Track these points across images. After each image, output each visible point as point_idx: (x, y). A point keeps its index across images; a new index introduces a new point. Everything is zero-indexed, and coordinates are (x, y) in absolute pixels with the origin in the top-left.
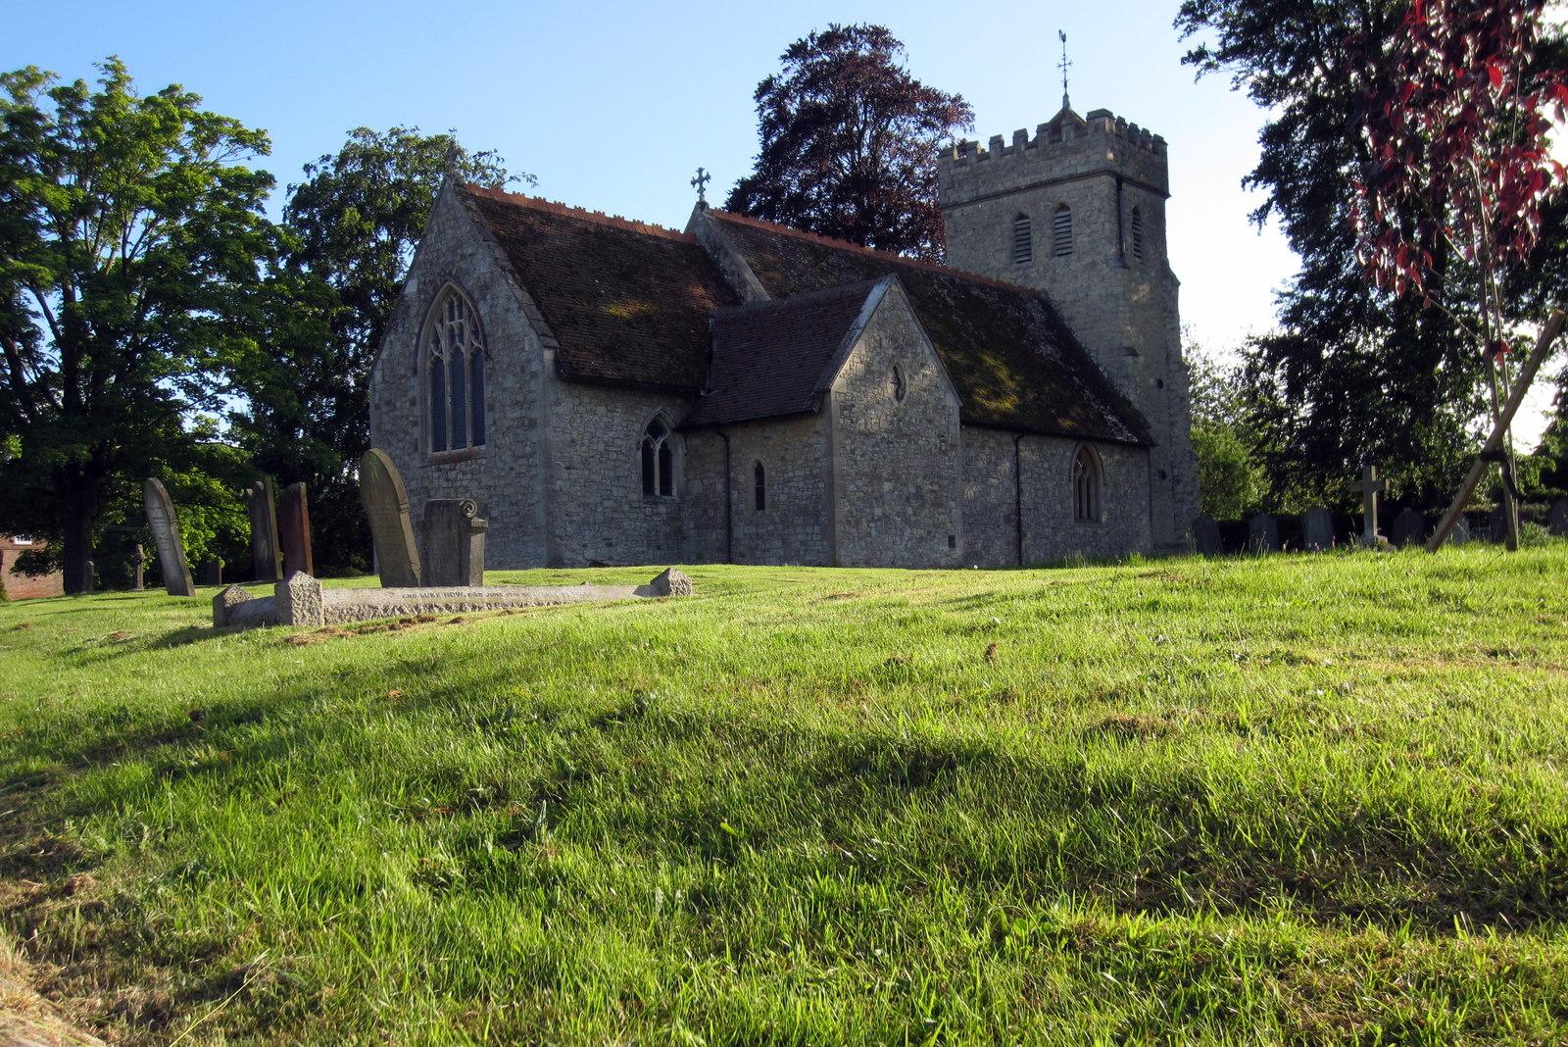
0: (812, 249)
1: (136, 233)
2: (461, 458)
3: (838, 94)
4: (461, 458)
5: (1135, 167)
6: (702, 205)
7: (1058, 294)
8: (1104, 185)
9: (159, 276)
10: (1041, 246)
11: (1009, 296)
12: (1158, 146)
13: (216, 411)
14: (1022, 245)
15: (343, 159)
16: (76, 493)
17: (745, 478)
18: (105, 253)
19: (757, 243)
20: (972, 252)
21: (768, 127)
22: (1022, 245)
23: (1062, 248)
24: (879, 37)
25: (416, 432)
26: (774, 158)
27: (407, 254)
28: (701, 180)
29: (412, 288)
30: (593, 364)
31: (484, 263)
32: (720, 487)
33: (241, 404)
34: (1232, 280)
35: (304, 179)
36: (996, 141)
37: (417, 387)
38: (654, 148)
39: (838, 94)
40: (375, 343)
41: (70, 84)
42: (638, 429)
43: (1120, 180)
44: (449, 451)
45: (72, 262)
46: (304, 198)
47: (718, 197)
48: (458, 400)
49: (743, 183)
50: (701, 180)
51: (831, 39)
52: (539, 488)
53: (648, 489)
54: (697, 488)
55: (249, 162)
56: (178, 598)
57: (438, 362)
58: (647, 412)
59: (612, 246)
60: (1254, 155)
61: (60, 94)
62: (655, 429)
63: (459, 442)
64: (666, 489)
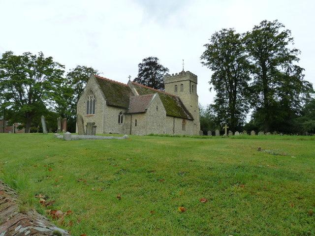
0: (145, 88)
1: (42, 79)
2: (91, 116)
3: (150, 67)
4: (91, 116)
5: (193, 79)
6: (130, 81)
7: (181, 98)
8: (188, 82)
9: (46, 86)
10: (179, 90)
11: (174, 97)
12: (196, 77)
13: (51, 105)
14: (176, 90)
15: (76, 69)
16: (30, 117)
17: (134, 121)
18: (37, 81)
19: (137, 87)
20: (169, 90)
21: (140, 71)
22: (176, 90)
23: (182, 91)
24: (156, 59)
25: (84, 111)
26: (140, 75)
27: (84, 85)
28: (130, 77)
29: (85, 90)
30: (111, 103)
31: (96, 87)
32: (130, 123)
33: (56, 105)
34: (206, 96)
35: (69, 72)
36: (173, 74)
37: (85, 105)
38: (123, 71)
39: (150, 67)
40: (78, 97)
41: (34, 55)
42: (118, 114)
43: (191, 81)
44: (89, 115)
45: (30, 82)
46: (69, 74)
47: (132, 80)
48: (91, 107)
49: (136, 78)
50: (130, 77)
51: (150, 58)
52: (103, 121)
53: (119, 122)
54: (126, 123)
55: (62, 69)
56: (205, 136)
57: (88, 101)
58: (119, 111)
59: (116, 86)
60: (210, 79)
61: (32, 57)
62: (121, 113)
63: (91, 113)
64: (122, 123)
